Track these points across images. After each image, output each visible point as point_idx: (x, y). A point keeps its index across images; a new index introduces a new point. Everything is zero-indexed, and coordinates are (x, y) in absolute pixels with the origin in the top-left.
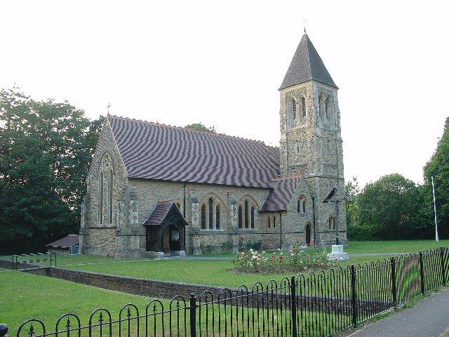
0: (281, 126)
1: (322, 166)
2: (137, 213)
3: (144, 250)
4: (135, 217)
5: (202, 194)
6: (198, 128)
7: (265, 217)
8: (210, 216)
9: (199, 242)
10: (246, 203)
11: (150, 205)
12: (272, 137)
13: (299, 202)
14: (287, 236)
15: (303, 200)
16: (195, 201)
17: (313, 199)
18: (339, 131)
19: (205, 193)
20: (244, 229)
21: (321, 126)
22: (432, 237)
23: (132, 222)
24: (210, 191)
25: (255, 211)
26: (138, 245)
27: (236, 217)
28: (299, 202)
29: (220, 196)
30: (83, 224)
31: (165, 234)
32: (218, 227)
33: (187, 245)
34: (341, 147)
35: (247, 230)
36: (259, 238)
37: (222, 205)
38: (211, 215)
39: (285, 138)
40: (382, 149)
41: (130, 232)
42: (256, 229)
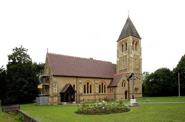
1: (133, 69)
2: (56, 89)
7: (110, 89)
10: (102, 84)
12: (114, 60)
14: (117, 95)
15: (124, 82)
16: (81, 83)
18: (141, 55)
19: (85, 81)
20: (101, 93)
22: (177, 95)
23: (54, 92)
25: (106, 87)
28: (123, 83)
29: (92, 82)
31: (68, 95)
32: (91, 92)
33: (76, 100)
34: (141, 62)
35: (102, 93)
38: (88, 88)
40: (157, 57)
41: (53, 96)
42: (106, 93)
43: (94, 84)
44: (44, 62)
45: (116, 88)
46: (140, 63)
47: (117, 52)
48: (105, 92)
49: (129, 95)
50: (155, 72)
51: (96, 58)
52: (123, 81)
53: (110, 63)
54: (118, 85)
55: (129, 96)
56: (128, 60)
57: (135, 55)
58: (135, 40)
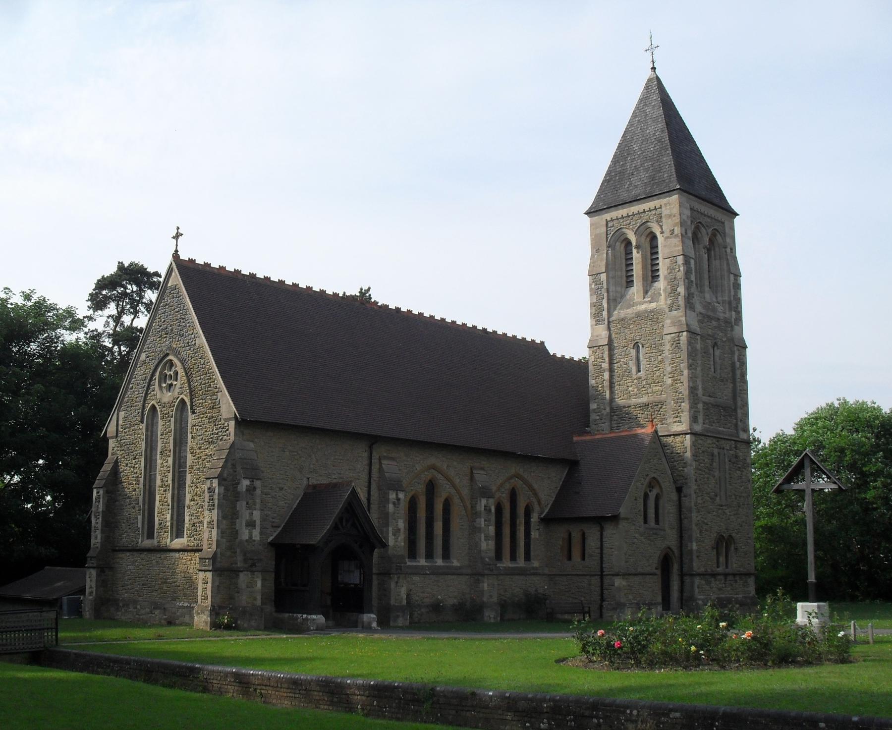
0: (593, 305)
1: (700, 406)
2: (257, 515)
3: (269, 608)
4: (251, 524)
5: (408, 469)
6: (362, 301)
7: (560, 532)
8: (430, 518)
9: (403, 591)
10: (513, 496)
11: (288, 496)
12: (567, 331)
13: (646, 496)
14: (618, 582)
16: (396, 486)
17: (679, 490)
20: (506, 563)
21: (699, 308)
23: (245, 534)
24: (513, 471)
25: (535, 518)
26: (259, 597)
27: (492, 530)
28: (646, 496)
29: (454, 473)
30: (96, 539)
36: (540, 585)
37: (456, 500)
39: (604, 334)
42: (536, 564)
43: (465, 492)
44: (144, 326)
45: (609, 530)
46: (738, 372)
47: (587, 280)
48: (528, 557)
49: (687, 580)
50: (801, 427)
51: (389, 295)
52: (651, 486)
53: (532, 353)
54: (623, 511)
55: (682, 591)
56: (667, 347)
57: (710, 318)
58: (704, 220)
